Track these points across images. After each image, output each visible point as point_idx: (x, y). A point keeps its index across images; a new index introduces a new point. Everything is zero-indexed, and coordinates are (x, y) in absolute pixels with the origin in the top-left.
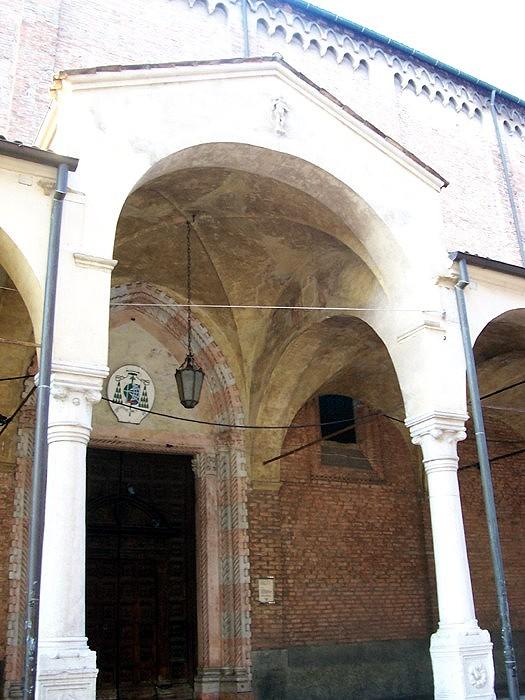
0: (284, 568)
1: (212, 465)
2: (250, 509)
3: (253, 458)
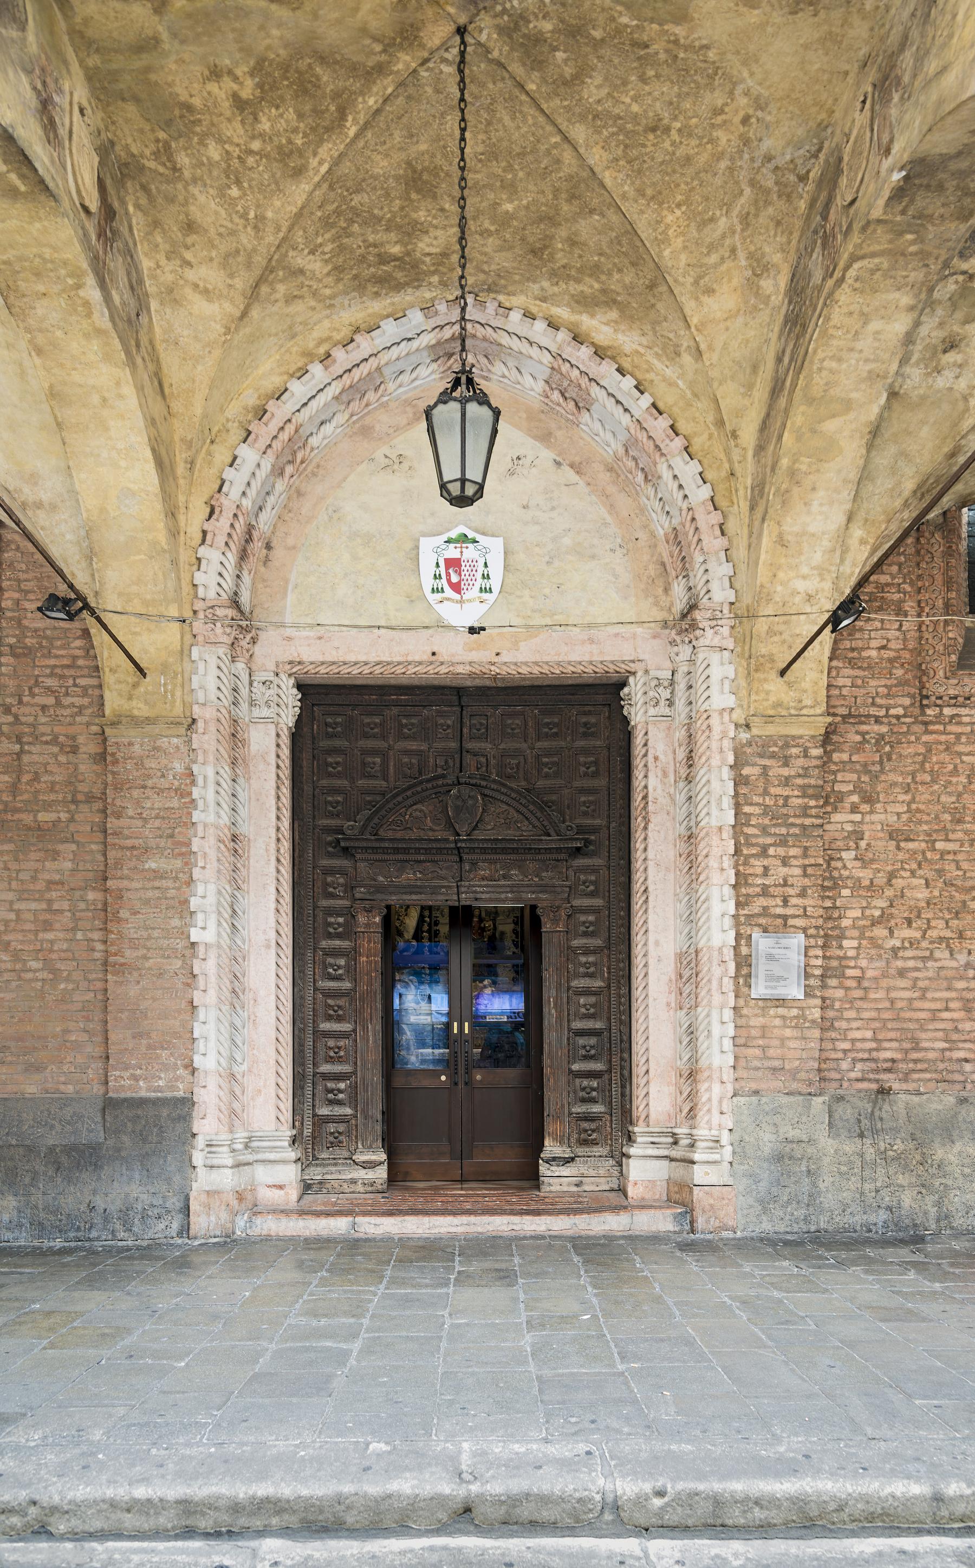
0: (831, 915)
1: (666, 694)
2: (740, 781)
3: (752, 665)
